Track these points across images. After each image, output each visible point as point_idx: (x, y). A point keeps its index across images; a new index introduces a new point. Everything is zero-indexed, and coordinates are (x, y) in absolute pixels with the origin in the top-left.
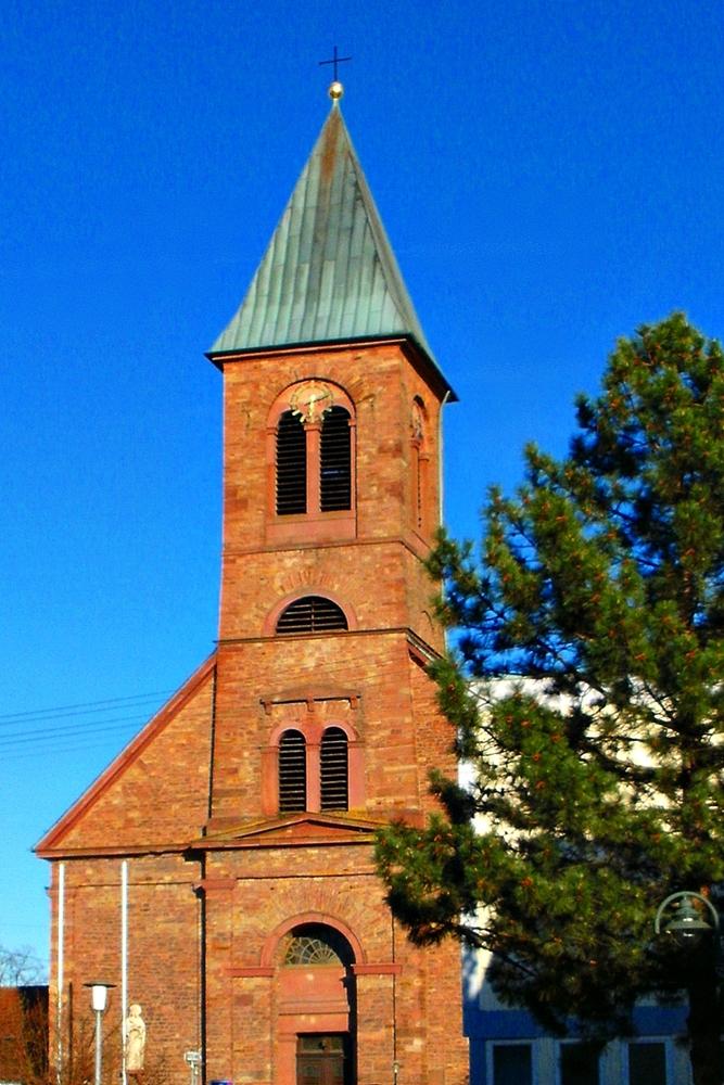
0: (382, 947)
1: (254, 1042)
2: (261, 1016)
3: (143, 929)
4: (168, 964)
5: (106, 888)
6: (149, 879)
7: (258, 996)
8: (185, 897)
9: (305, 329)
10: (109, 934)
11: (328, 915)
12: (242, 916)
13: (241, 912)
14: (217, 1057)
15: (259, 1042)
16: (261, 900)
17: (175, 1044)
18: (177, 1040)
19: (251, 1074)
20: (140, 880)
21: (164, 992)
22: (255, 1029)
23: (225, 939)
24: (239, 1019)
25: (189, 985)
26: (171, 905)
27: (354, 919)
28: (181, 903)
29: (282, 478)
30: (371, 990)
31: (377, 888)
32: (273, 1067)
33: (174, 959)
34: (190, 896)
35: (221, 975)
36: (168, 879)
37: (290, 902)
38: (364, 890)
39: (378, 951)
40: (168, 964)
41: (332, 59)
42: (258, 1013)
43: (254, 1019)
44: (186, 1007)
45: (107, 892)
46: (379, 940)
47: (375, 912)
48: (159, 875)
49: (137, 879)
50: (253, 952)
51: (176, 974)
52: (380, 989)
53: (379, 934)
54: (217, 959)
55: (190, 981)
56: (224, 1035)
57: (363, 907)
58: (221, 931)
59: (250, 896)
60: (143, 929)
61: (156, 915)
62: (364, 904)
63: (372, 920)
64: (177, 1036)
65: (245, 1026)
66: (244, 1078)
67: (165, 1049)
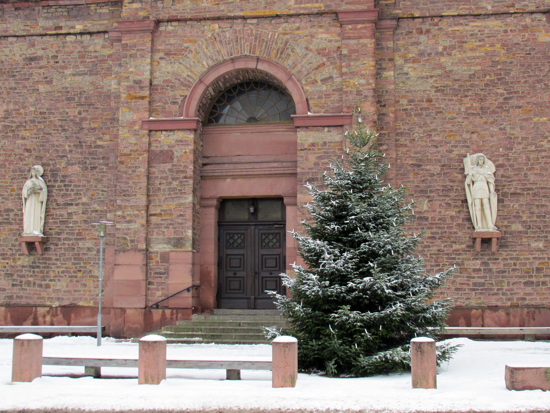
0: (328, 96)
1: (172, 205)
2: (182, 175)
3: (50, 82)
4: (78, 120)
5: (10, 39)
6: (61, 28)
7: (178, 152)
8: (98, 48)
9: (244, 161)
10: (11, 89)
11: (264, 61)
12: (163, 63)
13: (161, 58)
14: (129, 222)
15: (180, 205)
16: (186, 45)
17: (79, 209)
18: (83, 204)
19: (168, 241)
20: (48, 29)
21: (71, 151)
22: (174, 189)
23: (141, 88)
24: (156, 177)
25: (99, 143)
26: (82, 57)
27: (295, 65)
28: (93, 54)
29: (82, 335)
30: (313, 145)
31: (321, 30)
32: (194, 234)
33: (83, 115)
34: (103, 47)
35: (137, 127)
36: (79, 27)
37: (218, 46)
38: (307, 32)
39: (323, 101)
40: (78, 120)
41: (143, 306)
42: (178, 172)
43: (174, 179)
44: (95, 168)
45: (11, 43)
46: (324, 88)
47: (319, 58)
48: (70, 23)
49: (44, 28)
50: (174, 103)
51: (86, 131)
52: (325, 143)
53: (324, 81)
54: (130, 109)
55: (100, 139)
56: (138, 196)
57: (304, 51)
58: (139, 78)
59: (172, 41)
60: (50, 82)
61: (65, 68)
62: (307, 48)
63: (315, 65)
64: (84, 200)
65: (162, 187)
66: (161, 246)
67: (70, 214)
